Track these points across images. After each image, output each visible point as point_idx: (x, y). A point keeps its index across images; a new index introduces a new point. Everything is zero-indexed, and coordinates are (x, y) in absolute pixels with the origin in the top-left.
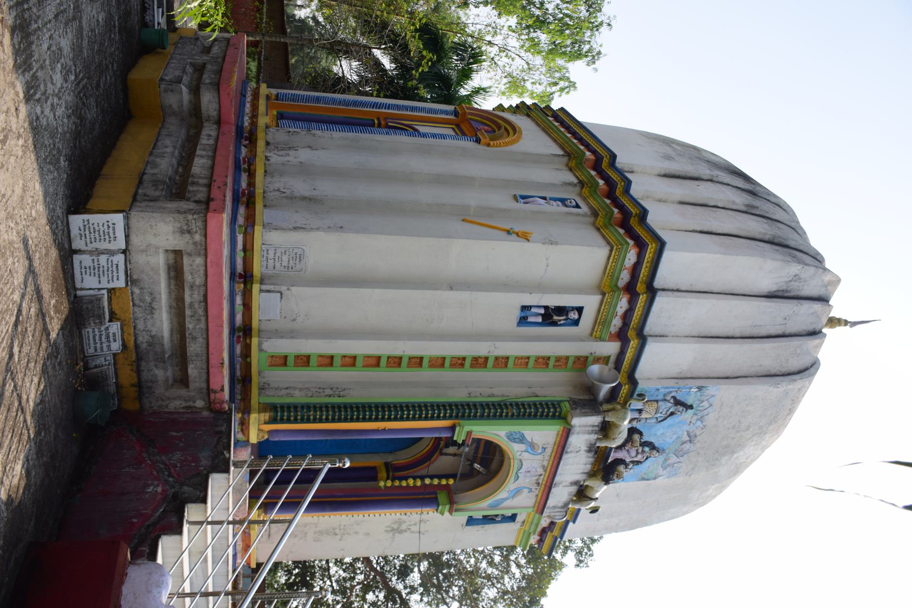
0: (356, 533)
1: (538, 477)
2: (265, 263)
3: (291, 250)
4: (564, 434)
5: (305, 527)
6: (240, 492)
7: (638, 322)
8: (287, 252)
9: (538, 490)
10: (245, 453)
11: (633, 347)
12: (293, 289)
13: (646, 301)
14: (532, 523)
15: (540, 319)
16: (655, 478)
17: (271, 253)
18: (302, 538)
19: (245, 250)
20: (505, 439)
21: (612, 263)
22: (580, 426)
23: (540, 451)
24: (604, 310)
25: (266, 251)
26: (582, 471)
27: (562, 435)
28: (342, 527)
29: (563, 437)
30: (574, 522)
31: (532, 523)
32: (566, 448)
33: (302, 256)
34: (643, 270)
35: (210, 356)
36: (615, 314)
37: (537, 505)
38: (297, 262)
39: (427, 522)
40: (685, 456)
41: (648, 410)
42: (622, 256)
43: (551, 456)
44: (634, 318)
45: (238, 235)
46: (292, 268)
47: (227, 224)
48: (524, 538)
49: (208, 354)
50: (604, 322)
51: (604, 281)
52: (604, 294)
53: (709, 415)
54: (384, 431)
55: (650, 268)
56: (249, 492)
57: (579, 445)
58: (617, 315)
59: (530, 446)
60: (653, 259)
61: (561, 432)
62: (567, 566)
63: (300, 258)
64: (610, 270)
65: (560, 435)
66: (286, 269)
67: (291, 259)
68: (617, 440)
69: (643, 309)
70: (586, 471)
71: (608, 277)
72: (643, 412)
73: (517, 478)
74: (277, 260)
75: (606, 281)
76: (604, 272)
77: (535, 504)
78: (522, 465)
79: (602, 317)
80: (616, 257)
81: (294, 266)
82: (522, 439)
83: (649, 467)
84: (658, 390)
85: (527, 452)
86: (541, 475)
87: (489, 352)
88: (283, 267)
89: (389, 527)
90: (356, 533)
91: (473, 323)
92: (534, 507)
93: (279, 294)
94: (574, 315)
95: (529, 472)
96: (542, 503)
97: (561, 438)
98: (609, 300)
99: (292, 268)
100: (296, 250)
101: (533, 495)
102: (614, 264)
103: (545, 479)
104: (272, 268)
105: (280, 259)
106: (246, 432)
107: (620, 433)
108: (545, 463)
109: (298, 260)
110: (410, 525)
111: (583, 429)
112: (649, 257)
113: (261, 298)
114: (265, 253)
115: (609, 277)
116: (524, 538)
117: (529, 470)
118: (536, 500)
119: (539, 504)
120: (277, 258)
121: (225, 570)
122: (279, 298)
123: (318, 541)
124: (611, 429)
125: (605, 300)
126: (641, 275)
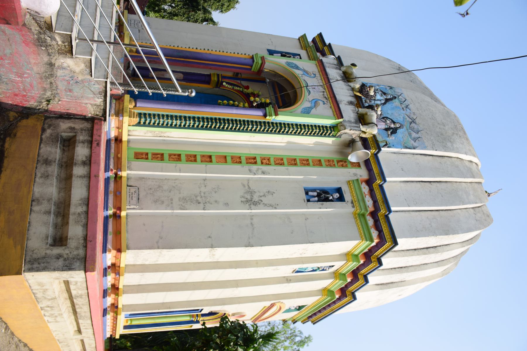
0: (216, 202)
9: (329, 103)
14: (358, 200)
26: (349, 95)
27: (319, 65)
28: (202, 194)
29: (321, 65)
31: (358, 200)
34: (319, 45)
37: (335, 114)
39: (274, 194)
43: (322, 79)
47: (103, 153)
60: (320, 40)
61: (317, 64)
73: (309, 92)
74: (135, 25)
77: (334, 114)
79: (311, 57)
83: (403, 138)
89: (243, 197)
96: (337, 110)
97: (320, 67)
103: (328, 94)
110: (261, 197)
111: (332, 65)
119: (336, 112)
125: (308, 51)
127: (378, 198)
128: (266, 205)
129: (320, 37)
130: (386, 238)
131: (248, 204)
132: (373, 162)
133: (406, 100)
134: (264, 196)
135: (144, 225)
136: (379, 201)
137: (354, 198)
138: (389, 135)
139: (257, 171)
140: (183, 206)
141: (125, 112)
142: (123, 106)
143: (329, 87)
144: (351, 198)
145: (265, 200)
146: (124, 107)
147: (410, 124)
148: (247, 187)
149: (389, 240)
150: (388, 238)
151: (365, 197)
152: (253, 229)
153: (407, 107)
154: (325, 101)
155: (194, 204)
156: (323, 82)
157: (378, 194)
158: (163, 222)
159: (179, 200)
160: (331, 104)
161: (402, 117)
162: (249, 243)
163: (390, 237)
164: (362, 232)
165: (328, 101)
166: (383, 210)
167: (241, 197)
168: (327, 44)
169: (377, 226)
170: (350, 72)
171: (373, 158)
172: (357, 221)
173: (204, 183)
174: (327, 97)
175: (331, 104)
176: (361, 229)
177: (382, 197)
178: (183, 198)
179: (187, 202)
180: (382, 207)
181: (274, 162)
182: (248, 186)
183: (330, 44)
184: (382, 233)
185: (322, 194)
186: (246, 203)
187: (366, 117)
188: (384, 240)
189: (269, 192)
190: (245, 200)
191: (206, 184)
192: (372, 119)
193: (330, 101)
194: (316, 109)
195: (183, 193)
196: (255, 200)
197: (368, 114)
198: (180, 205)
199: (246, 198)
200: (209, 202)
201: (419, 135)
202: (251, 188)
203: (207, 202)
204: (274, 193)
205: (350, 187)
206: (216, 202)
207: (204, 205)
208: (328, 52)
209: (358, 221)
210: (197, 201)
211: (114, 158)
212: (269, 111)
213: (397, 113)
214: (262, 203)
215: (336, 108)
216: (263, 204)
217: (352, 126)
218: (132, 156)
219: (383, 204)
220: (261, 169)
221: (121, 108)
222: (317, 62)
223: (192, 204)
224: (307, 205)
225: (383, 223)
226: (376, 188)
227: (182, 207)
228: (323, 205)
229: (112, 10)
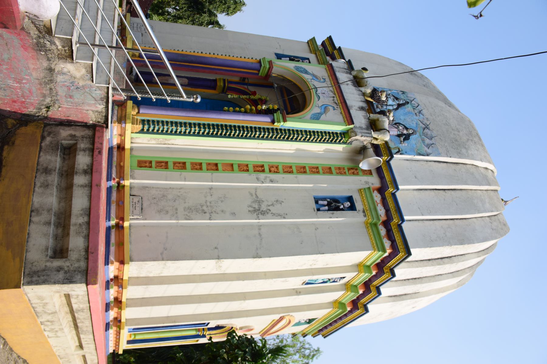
0: (222, 211)
1: (332, 99)
4: (330, 68)
5: (175, 201)
6: (119, 74)
14: (370, 209)
26: (360, 100)
27: (329, 69)
28: (208, 204)
31: (370, 209)
34: (329, 49)
35: (76, 315)
37: (346, 120)
39: (282, 203)
42: (314, 41)
48: (377, 239)
56: (123, 92)
61: (327, 69)
65: (328, 70)
74: (138, 28)
77: (344, 120)
83: (416, 144)
89: (250, 206)
96: (348, 116)
103: (338, 99)
110: (269, 206)
114: (132, 24)
116: (377, 239)
118: (343, 116)
119: (346, 117)
122: (141, 35)
127: (390, 207)
128: (274, 214)
131: (255, 214)
134: (273, 205)
135: (148, 235)
136: (391, 210)
137: (365, 206)
139: (265, 179)
140: (188, 216)
141: (128, 118)
142: (126, 113)
143: (339, 92)
145: (273, 209)
146: (127, 114)
148: (254, 196)
149: (402, 250)
150: (401, 248)
151: (377, 206)
152: (261, 239)
154: (335, 106)
155: (199, 213)
157: (391, 205)
159: (184, 210)
162: (257, 254)
163: (404, 247)
165: (338, 107)
168: (337, 48)
169: (390, 236)
171: (385, 165)
172: (369, 231)
173: (210, 193)
174: (337, 102)
176: (373, 239)
177: (394, 206)
179: (192, 212)
180: (395, 216)
181: (282, 170)
182: (256, 194)
183: (340, 48)
184: (395, 243)
186: (254, 213)
187: (377, 123)
189: (277, 201)
190: (253, 209)
191: (212, 194)
192: (383, 125)
193: (341, 106)
194: (326, 114)
196: (263, 210)
197: (380, 120)
198: (185, 215)
199: (254, 208)
205: (362, 196)
206: (222, 211)
207: (211, 215)
209: (370, 231)
210: (203, 210)
211: (116, 166)
212: (277, 117)
214: (270, 212)
216: (272, 213)
217: (363, 133)
218: (136, 164)
219: (396, 213)
221: (124, 115)
223: (197, 213)
225: (396, 232)
226: (388, 196)
228: (334, 215)
229: (114, 13)
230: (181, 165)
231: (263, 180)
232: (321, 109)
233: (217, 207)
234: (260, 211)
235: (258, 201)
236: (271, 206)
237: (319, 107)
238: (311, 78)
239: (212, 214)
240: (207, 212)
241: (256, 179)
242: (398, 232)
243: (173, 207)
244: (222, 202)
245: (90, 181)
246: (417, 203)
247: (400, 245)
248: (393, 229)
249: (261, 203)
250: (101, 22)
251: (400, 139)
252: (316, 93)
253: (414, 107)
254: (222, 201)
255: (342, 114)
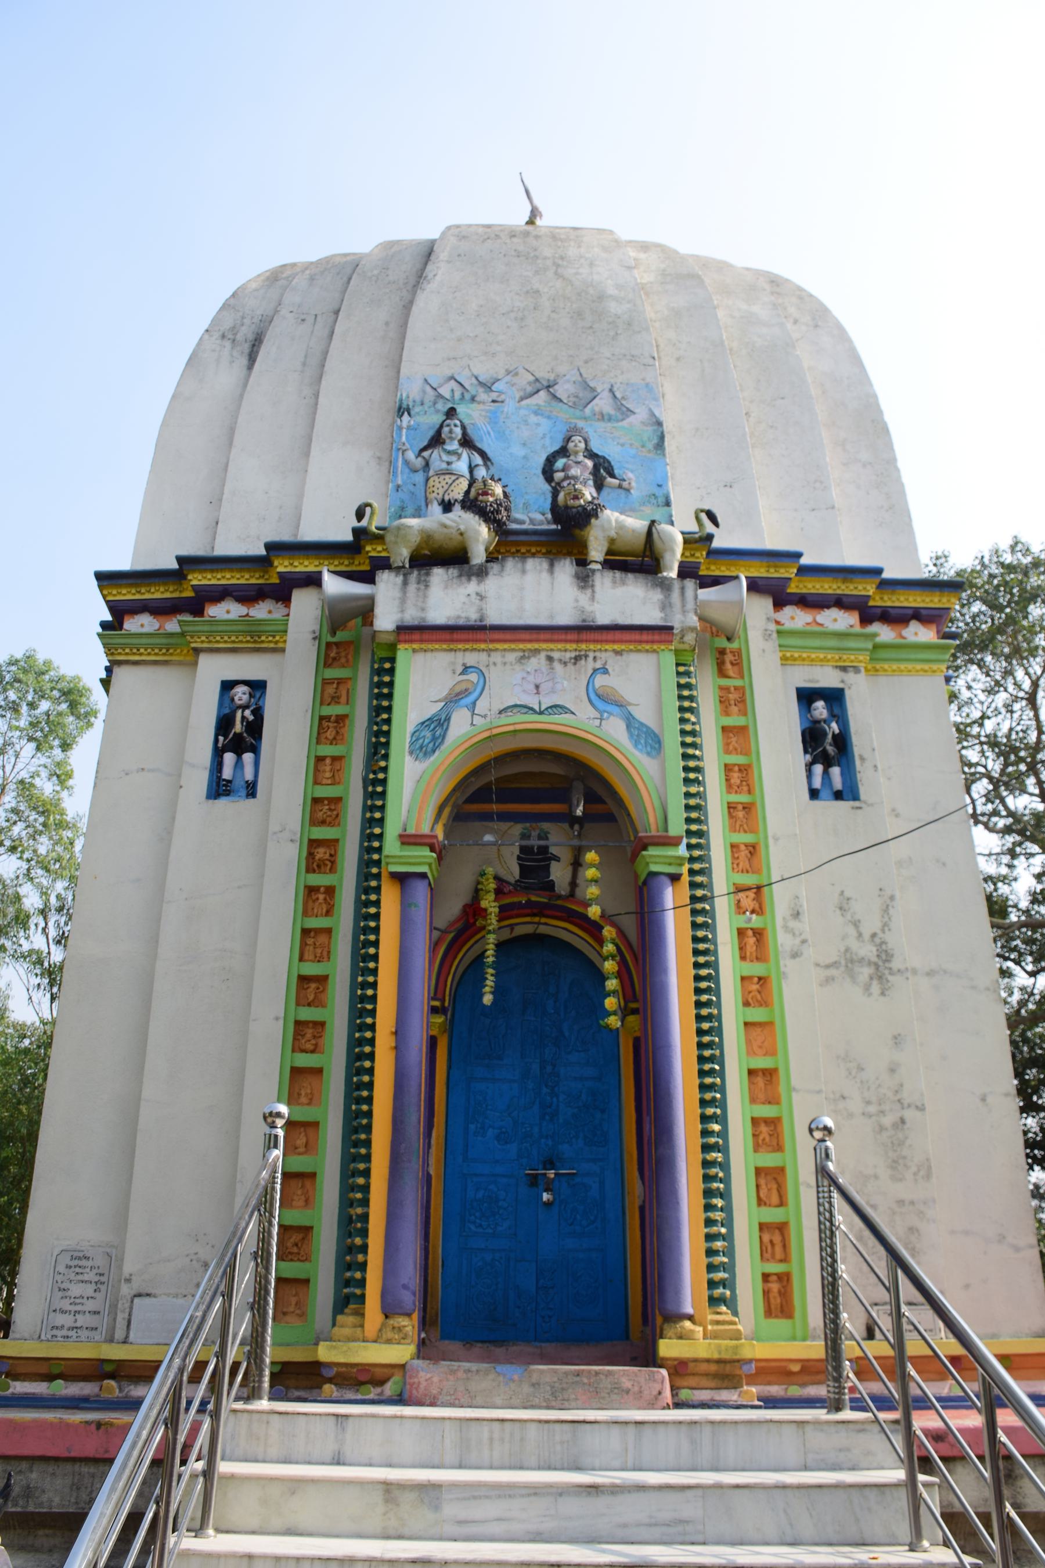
0: (892, 1071)
2: (84, 1334)
3: (59, 1278)
7: (249, 570)
8: (63, 1286)
9: (598, 654)
10: (422, 1374)
11: (291, 564)
12: (128, 1268)
13: (201, 571)
14: (839, 649)
15: (248, 757)
16: (659, 424)
17: (61, 1319)
18: (921, 1214)
19: (50, 1378)
20: (432, 758)
21: (141, 654)
22: (402, 611)
23: (473, 677)
24: (226, 642)
25: (55, 1332)
26: (545, 575)
27: (421, 641)
28: (872, 1109)
30: (798, 555)
31: (839, 649)
32: (472, 623)
33: (76, 1254)
35: (73, 1454)
36: (245, 619)
37: (648, 647)
38: (89, 1263)
39: (847, 894)
40: (592, 384)
41: (441, 491)
44: (242, 581)
45: (11, 1390)
46: (101, 1275)
48: (913, 656)
49: (74, 1460)
50: (252, 634)
51: (181, 658)
52: (197, 651)
53: (475, 373)
54: (399, 1033)
55: (149, 585)
57: (463, 599)
58: (247, 615)
59: (456, 701)
60: (131, 585)
61: (415, 646)
62: (1016, 537)
63: (80, 1258)
64: (156, 654)
65: (423, 646)
66: (103, 1288)
67: (80, 1277)
68: (462, 528)
69: (217, 571)
70: (545, 565)
71: (171, 654)
72: (447, 498)
73: (557, 708)
74: (78, 1308)
75: (179, 654)
76: (165, 663)
77: (647, 651)
78: (516, 706)
79: (241, 642)
80: (127, 650)
81: (95, 1271)
82: (438, 724)
83: (623, 445)
84: (398, 488)
85: (474, 703)
86: (550, 659)
87: (292, 841)
88: (97, 1295)
89: (867, 988)
90: (892, 1071)
91: (239, 887)
92: (654, 651)
93: (136, 1300)
94: (241, 694)
95: (537, 687)
96: (636, 636)
98: (203, 638)
99: (101, 1275)
100: (61, 1268)
101: (614, 663)
102: (142, 650)
103: (560, 646)
104: (97, 1316)
105: (77, 1301)
106: (379, 1373)
107: (445, 526)
108: (511, 657)
109: (84, 1263)
112: (129, 592)
113: (139, 1341)
114: (59, 1333)
115: (171, 651)
116: (913, 656)
117: (532, 687)
118: (631, 650)
119: (640, 642)
120: (73, 1308)
121: (616, 1430)
123: (930, 1168)
124: (440, 547)
126: (168, 595)
127: (830, 592)
128: (885, 925)
129: (120, 582)
130: (937, 606)
131: (890, 978)
132: (728, 569)
133: (452, 378)
134: (856, 924)
135: (967, 1286)
136: (839, 592)
137: (828, 661)
138: (620, 487)
139: (794, 934)
140: (919, 1170)
141: (736, 1354)
143: (534, 636)
144: (830, 669)
145: (871, 924)
146: (716, 1356)
147: (561, 401)
148: (833, 972)
149: (944, 600)
151: (821, 625)
152: (945, 972)
153: (487, 387)
154: (590, 665)
155: (906, 1138)
156: (505, 650)
157: (818, 586)
158: (953, 1232)
159: (901, 1180)
160: (606, 650)
161: (533, 419)
162: (988, 989)
163: (938, 593)
164: (919, 666)
165: (591, 655)
166: (869, 587)
167: (870, 995)
170: (418, 540)
171: (715, 564)
172: (885, 670)
174: (573, 655)
175: (606, 650)
176: (910, 666)
177: (830, 579)
178: (893, 1168)
179: (905, 1158)
180: (860, 587)
181: (745, 874)
182: (828, 967)
183: (180, 560)
184: (924, 612)
185: (825, 751)
186: (888, 981)
187: (619, 546)
188: (942, 612)
189: (841, 908)
190: (875, 982)
193: (592, 647)
194: (630, 704)
195: (875, 1167)
197: (613, 534)
198: (916, 1180)
199: (871, 978)
200: (897, 1092)
201: (601, 387)
202: (835, 959)
203: (898, 1097)
204: (842, 892)
205: (795, 659)
207: (909, 1106)
208: (219, 576)
209: (886, 666)
210: (895, 1126)
211: (803, 1385)
212: (665, 863)
213: (518, 428)
214: (881, 935)
215: (627, 636)
216: (883, 931)
217: (683, 606)
218: (781, 1325)
220: (784, 919)
221: (713, 1368)
222: (407, 646)
223: (908, 1142)
224: (872, 805)
225: (894, 598)
226: (797, 587)
227: (922, 1173)
228: (865, 756)
229: (534, 1426)
230: (762, 1182)
231: (797, 941)
232: (610, 714)
233: (879, 1086)
234: (881, 963)
235: (850, 965)
236: (862, 929)
237: (601, 719)
238: (465, 713)
239: (906, 1103)
240: (899, 1115)
241: (797, 959)
242: (893, 593)
243: (894, 1213)
244: (863, 1069)
245: (1036, 1460)
246: (796, 510)
247: (931, 601)
248: (883, 604)
249: (855, 958)
250: (350, 1465)
251: (610, 487)
252: (541, 713)
253: (467, 396)
254: (861, 1069)
255: (623, 650)
